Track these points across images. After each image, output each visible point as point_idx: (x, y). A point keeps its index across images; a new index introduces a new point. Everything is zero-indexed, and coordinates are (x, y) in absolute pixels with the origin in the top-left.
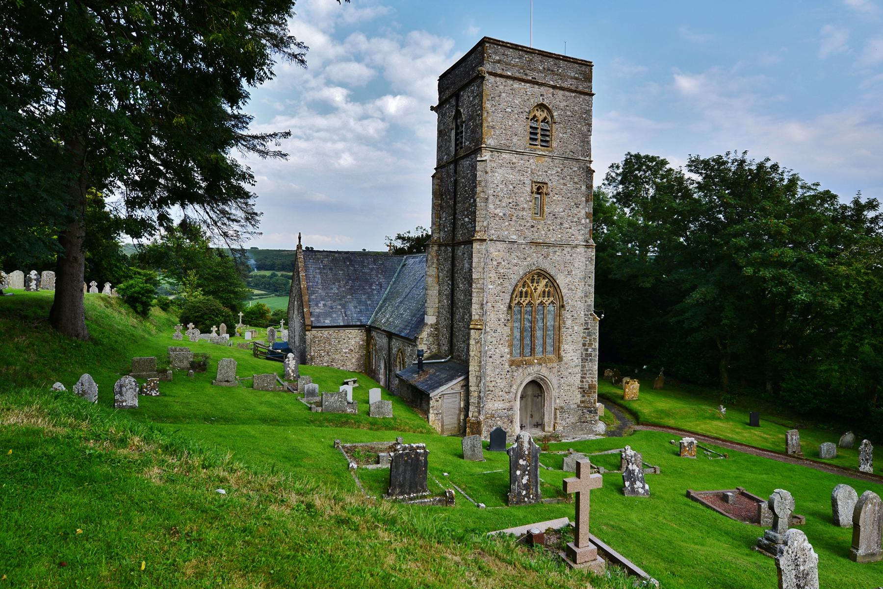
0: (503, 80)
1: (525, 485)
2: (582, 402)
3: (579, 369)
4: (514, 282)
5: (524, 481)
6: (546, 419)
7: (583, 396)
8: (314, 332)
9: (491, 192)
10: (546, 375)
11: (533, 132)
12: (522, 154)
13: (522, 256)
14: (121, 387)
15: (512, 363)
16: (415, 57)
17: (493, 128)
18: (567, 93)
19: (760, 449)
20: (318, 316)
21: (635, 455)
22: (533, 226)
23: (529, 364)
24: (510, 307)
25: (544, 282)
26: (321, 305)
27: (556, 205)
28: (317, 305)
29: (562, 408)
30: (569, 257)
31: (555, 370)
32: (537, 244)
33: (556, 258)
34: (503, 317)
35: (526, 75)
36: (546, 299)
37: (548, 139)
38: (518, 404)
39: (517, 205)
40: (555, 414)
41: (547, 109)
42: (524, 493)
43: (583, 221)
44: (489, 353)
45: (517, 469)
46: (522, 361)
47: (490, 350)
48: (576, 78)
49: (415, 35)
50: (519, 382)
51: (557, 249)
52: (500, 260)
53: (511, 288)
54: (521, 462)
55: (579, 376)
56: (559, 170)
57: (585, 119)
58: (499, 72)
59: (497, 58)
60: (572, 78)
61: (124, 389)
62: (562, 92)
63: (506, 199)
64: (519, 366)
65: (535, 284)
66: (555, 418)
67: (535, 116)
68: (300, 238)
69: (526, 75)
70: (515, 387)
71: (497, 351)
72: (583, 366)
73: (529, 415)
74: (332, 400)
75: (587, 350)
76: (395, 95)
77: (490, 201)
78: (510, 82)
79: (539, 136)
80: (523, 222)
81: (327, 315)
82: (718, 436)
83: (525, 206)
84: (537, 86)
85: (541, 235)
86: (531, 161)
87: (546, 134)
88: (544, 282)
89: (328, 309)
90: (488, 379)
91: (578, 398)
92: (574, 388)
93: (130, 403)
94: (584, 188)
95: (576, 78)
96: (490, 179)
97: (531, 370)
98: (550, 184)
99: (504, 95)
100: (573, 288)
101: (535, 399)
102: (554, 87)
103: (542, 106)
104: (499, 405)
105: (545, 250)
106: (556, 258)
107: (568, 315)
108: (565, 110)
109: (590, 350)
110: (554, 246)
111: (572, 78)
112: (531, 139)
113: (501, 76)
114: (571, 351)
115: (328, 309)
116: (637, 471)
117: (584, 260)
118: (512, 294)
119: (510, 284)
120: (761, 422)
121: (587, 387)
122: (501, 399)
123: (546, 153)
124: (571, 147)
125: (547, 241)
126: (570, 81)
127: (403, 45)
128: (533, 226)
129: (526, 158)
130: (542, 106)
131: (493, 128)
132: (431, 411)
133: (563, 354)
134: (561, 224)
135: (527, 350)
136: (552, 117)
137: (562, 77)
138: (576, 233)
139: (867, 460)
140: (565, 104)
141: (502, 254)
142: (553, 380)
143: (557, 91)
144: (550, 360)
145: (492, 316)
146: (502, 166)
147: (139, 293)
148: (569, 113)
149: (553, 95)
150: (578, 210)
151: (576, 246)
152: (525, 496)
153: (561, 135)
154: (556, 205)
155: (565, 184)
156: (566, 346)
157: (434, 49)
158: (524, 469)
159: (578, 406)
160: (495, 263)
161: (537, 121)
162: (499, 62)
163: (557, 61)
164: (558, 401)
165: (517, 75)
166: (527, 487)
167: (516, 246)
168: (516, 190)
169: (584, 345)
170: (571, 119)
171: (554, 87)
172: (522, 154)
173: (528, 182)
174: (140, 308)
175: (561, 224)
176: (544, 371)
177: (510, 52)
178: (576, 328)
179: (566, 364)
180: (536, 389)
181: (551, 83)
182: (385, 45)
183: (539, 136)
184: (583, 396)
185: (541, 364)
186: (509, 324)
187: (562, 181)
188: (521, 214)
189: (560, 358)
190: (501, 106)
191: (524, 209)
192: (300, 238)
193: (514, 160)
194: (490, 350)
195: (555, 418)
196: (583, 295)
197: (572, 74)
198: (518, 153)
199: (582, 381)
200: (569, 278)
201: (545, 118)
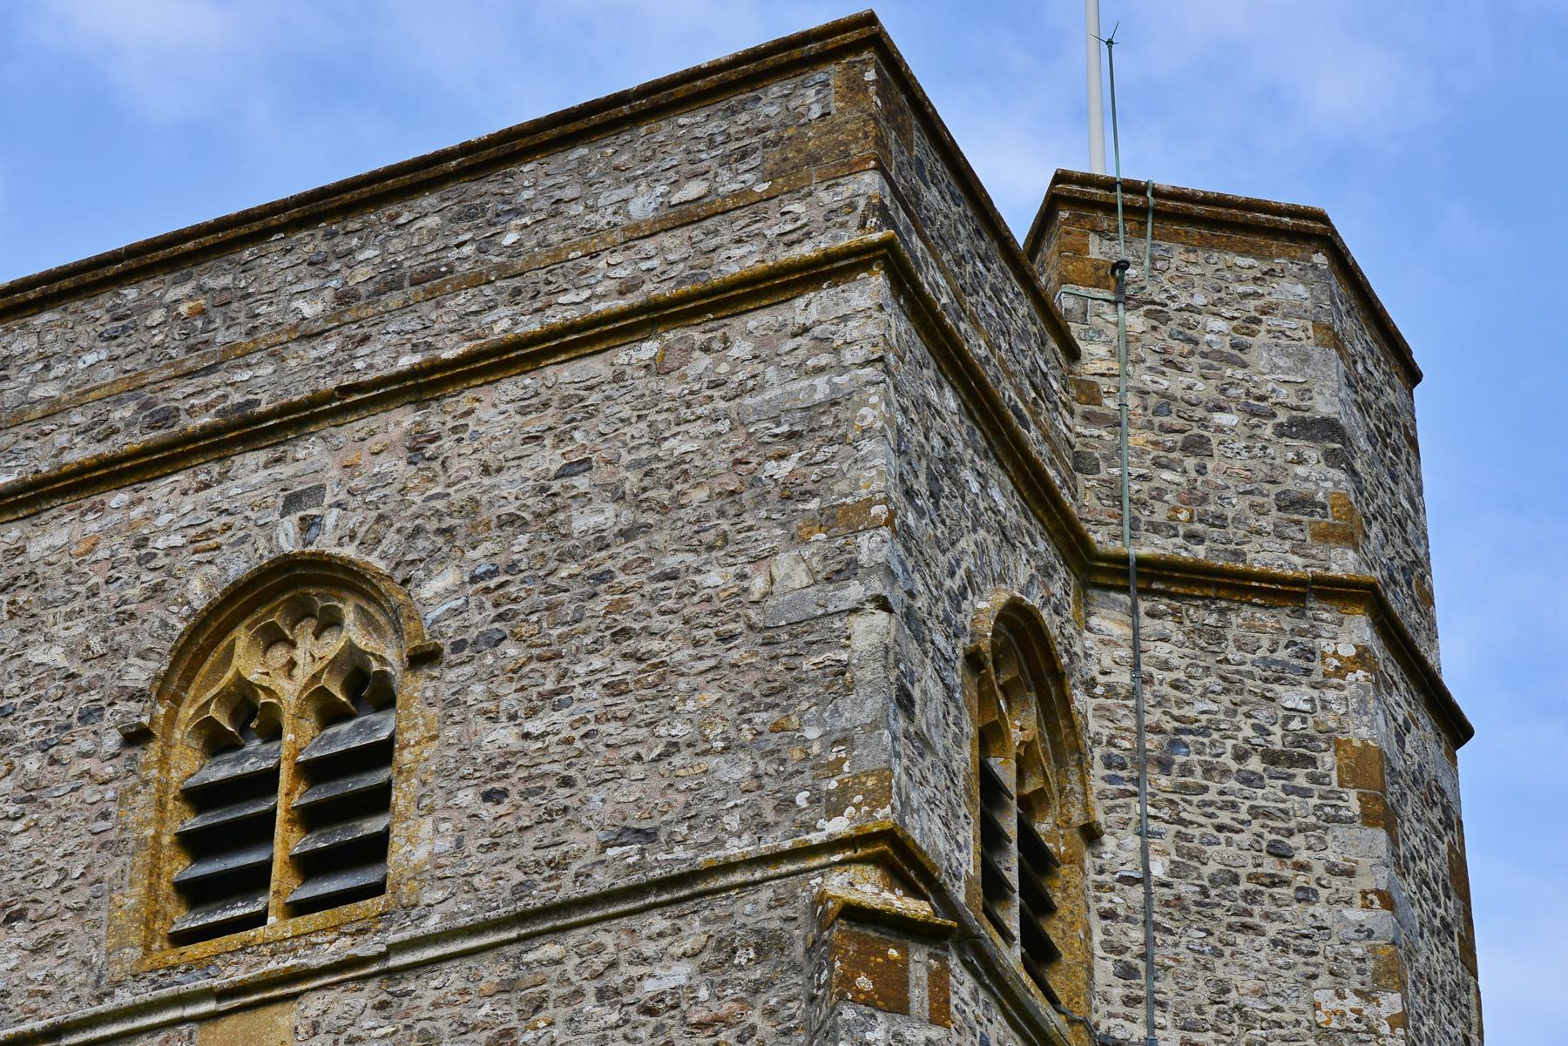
11: (224, 827)
18: (565, 374)
57: (791, 493)
79: (287, 841)
87: (352, 795)
102: (425, 384)
130: (295, 588)
140: (549, 459)
153: (505, 735)
171: (425, 384)
197: (643, 206)
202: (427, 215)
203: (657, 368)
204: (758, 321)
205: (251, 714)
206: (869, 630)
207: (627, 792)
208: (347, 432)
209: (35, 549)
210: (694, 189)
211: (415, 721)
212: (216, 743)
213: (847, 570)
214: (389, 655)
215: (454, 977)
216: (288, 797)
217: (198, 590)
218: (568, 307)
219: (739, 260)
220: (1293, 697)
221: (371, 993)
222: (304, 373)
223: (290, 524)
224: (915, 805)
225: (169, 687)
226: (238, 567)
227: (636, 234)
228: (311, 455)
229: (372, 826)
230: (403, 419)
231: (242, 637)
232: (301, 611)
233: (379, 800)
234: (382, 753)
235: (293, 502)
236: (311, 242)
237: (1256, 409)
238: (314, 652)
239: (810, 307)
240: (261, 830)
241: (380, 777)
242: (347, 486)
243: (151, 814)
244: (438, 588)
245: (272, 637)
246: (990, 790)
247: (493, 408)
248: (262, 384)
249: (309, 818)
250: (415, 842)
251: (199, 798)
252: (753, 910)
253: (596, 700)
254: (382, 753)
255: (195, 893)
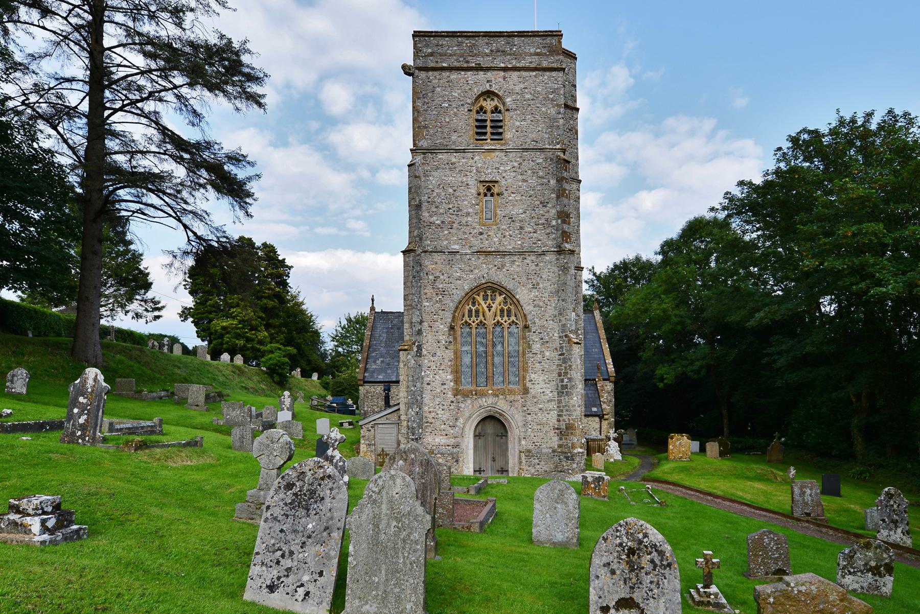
0: (436, 73)
1: (81, 425)
2: (560, 446)
3: (553, 405)
4: (457, 298)
5: (81, 421)
6: (510, 465)
7: (561, 439)
8: (367, 387)
9: (424, 198)
10: (504, 409)
11: (481, 125)
12: (464, 151)
13: (467, 268)
14: (13, 376)
15: (456, 393)
16: (672, 146)
17: (425, 127)
18: (524, 74)
19: (700, 492)
20: (373, 372)
21: (843, 577)
22: (481, 234)
23: (482, 395)
24: (452, 328)
25: (499, 299)
26: (379, 362)
27: (514, 205)
28: (375, 362)
29: (529, 451)
30: (534, 267)
31: (518, 404)
32: (488, 253)
33: (514, 269)
34: (443, 338)
35: (467, 62)
36: (506, 318)
37: (500, 130)
38: (469, 442)
39: (461, 210)
40: (520, 458)
41: (497, 95)
42: (79, 433)
43: (554, 223)
44: (427, 380)
45: (75, 406)
46: (471, 391)
47: (428, 376)
48: (537, 54)
49: (670, 122)
50: (467, 415)
51: (515, 258)
52: (437, 274)
53: (452, 305)
54: (81, 399)
55: (554, 414)
56: (516, 164)
57: (552, 100)
58: (432, 65)
59: (430, 50)
60: (531, 55)
61: (15, 378)
62: (517, 73)
63: (444, 205)
64: (468, 396)
65: (489, 301)
66: (520, 463)
67: (481, 108)
68: (373, 300)
69: (467, 62)
70: (461, 420)
71: (437, 377)
72: (559, 402)
73: (490, 457)
74: (234, 414)
75: (562, 381)
76: (650, 189)
77: (424, 208)
78: (446, 74)
79: (489, 130)
80: (467, 230)
81: (381, 371)
82: (711, 490)
83: (470, 210)
84: (482, 73)
85: (494, 242)
86: (477, 158)
87: (497, 126)
88: (499, 299)
89: (384, 365)
90: (426, 408)
91: (555, 441)
92: (547, 428)
93: (18, 390)
94: (553, 182)
95: (537, 54)
96: (423, 184)
97: (483, 401)
98: (503, 182)
99: (438, 89)
100: (541, 304)
101: (498, 439)
102: (505, 69)
103: (489, 94)
104: (440, 440)
105: (498, 260)
106: (514, 269)
107: (535, 338)
108: (522, 93)
109: (566, 380)
110: (511, 254)
111: (531, 55)
112: (477, 133)
113: (434, 69)
114: (541, 383)
115: (384, 365)
116: (338, 458)
117: (556, 269)
118: (455, 312)
119: (452, 301)
120: (844, 489)
121: (564, 427)
122: (444, 433)
123: (498, 147)
124: (534, 136)
125: (502, 249)
126: (529, 59)
127: (657, 135)
128: (481, 234)
129: (470, 155)
130: (489, 94)
131: (425, 127)
132: (362, 442)
133: (529, 385)
134: (521, 228)
135: (482, 380)
136: (504, 104)
137: (517, 56)
138: (544, 237)
139: (895, 522)
140: (522, 86)
141: (440, 267)
142: (515, 418)
143: (510, 73)
144: (511, 392)
145: (429, 337)
146: (438, 168)
147: (276, 365)
148: (528, 96)
149: (504, 79)
150: (545, 209)
151: (544, 253)
152: (79, 437)
153: (518, 123)
154: (514, 205)
155: (524, 181)
156: (533, 376)
157: (692, 133)
158: (83, 408)
159: (554, 451)
160: (431, 277)
161: (485, 112)
162: (431, 54)
163: (510, 39)
164: (523, 442)
165: (456, 64)
166: (83, 427)
167: (458, 257)
168: (457, 194)
169: (560, 375)
170: (533, 102)
171: (505, 69)
172: (464, 151)
173: (472, 182)
174: (277, 378)
175: (521, 228)
176: (502, 405)
177: (445, 41)
178: (547, 354)
179: (534, 397)
180: (493, 426)
181: (502, 65)
182: (637, 138)
183: (489, 130)
184: (561, 439)
185: (497, 396)
186: (452, 347)
187: (520, 177)
188: (464, 220)
189: (526, 391)
190: (434, 103)
191: (468, 214)
192: (373, 300)
193: (454, 160)
194: (428, 376)
195: (520, 463)
196: (556, 313)
197: (532, 50)
198: (457, 151)
199: (559, 421)
200: (535, 293)
201: (496, 108)
202: (502, 41)
203: (535, 76)
204: (548, 73)
205: (481, 110)
206: (561, 121)
207: (534, 136)
208: (496, 72)
209: (452, 77)
210: (539, 50)
213: (559, 113)
214: (501, 107)
215: (514, 154)
219: (545, 64)
221: (503, 154)
223: (488, 85)
225: (473, 104)
229: (500, 130)
230: (502, 73)
231: (481, 99)
232: (489, 97)
235: (488, 81)
236: (486, 40)
240: (485, 127)
243: (715, 571)
245: (485, 100)
247: (515, 75)
249: (491, 127)
250: (508, 135)
253: (529, 122)
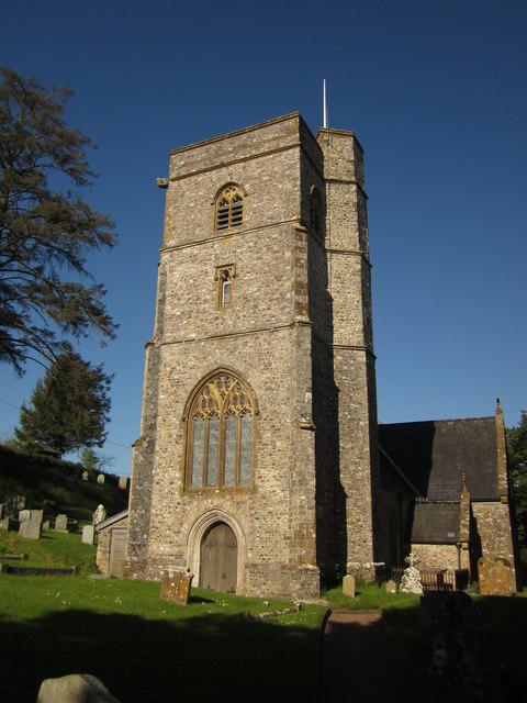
18: (261, 159)
87: (238, 211)
130: (229, 185)
204: (285, 153)
205: (225, 201)
211: (244, 202)
212: (221, 205)
214: (242, 194)
216: (230, 212)
217: (218, 186)
218: (262, 150)
219: (282, 145)
220: (347, 196)
222: (231, 157)
224: (264, 441)
225: (216, 198)
226: (223, 183)
227: (270, 140)
228: (231, 168)
233: (241, 213)
234: (241, 207)
237: (344, 159)
238: (232, 193)
239: (291, 151)
241: (500, 432)
242: (234, 173)
244: (247, 186)
246: (312, 211)
247: (253, 163)
248: (225, 159)
250: (245, 219)
251: (220, 212)
252: (285, 227)
254: (241, 207)
255: (220, 223)
